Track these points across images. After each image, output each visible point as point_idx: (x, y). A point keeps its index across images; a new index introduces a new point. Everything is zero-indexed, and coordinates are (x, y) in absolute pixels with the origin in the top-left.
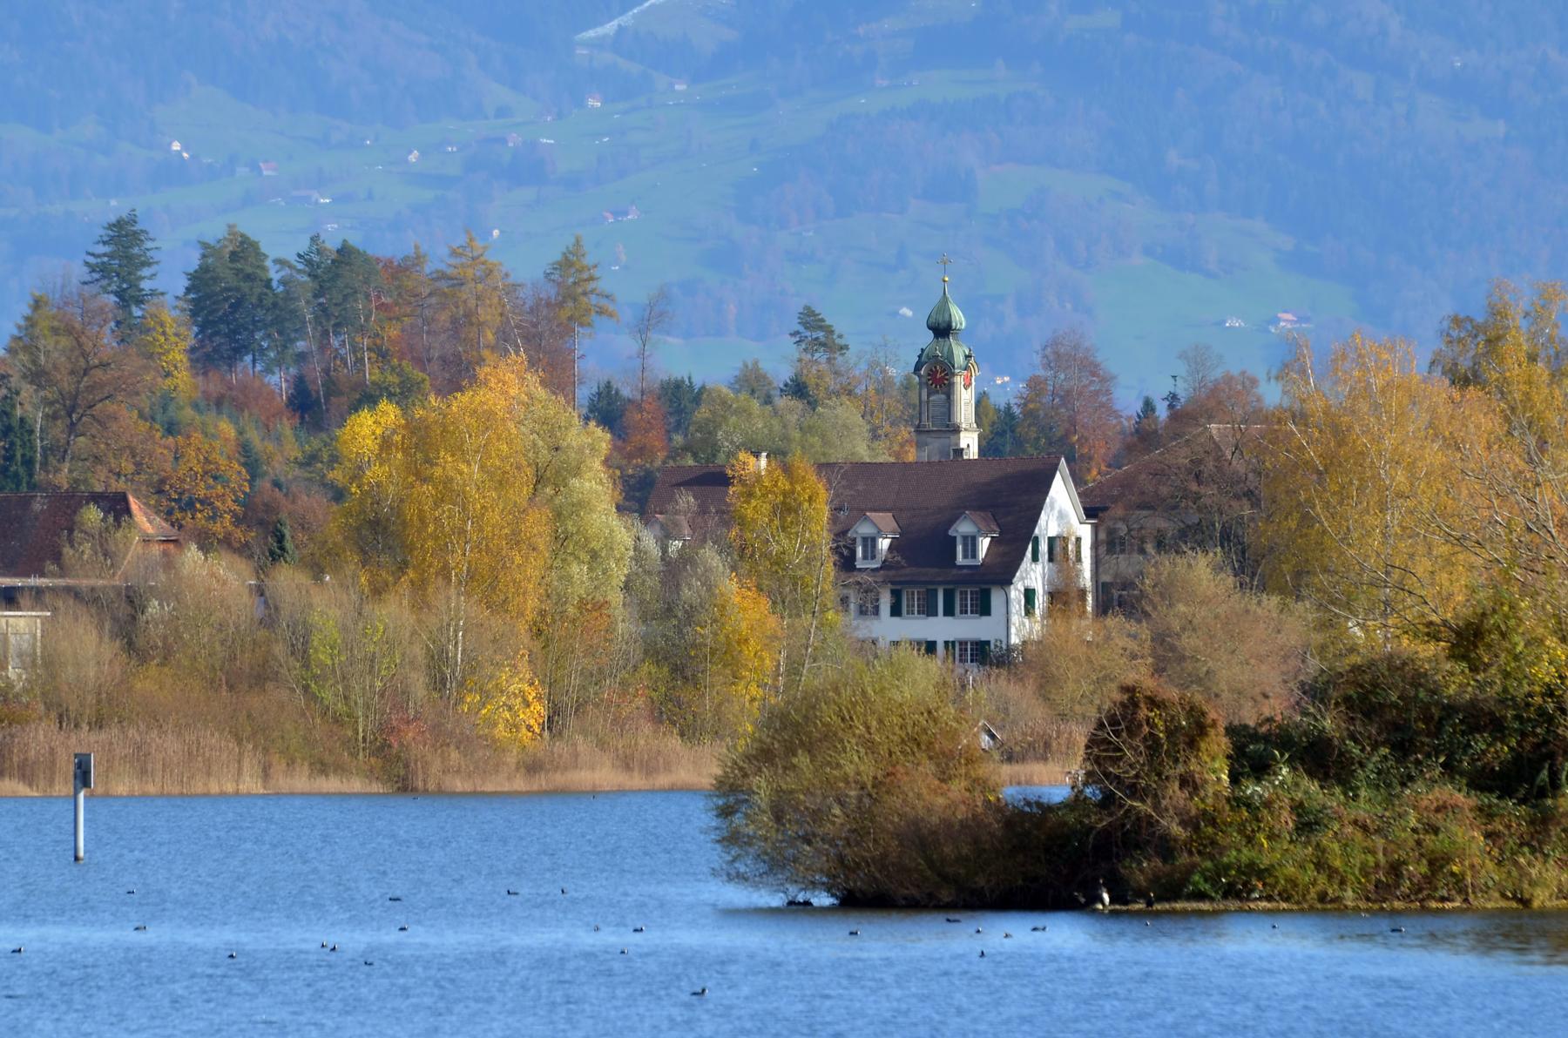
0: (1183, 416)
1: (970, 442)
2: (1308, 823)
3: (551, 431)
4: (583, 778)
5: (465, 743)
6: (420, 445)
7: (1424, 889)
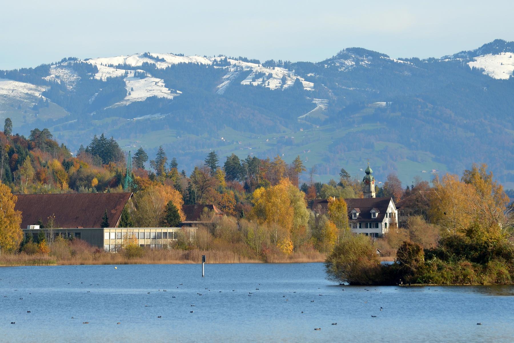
0: (414, 190)
1: (374, 195)
2: (440, 268)
4: (300, 260)
5: (278, 253)
6: (269, 195)
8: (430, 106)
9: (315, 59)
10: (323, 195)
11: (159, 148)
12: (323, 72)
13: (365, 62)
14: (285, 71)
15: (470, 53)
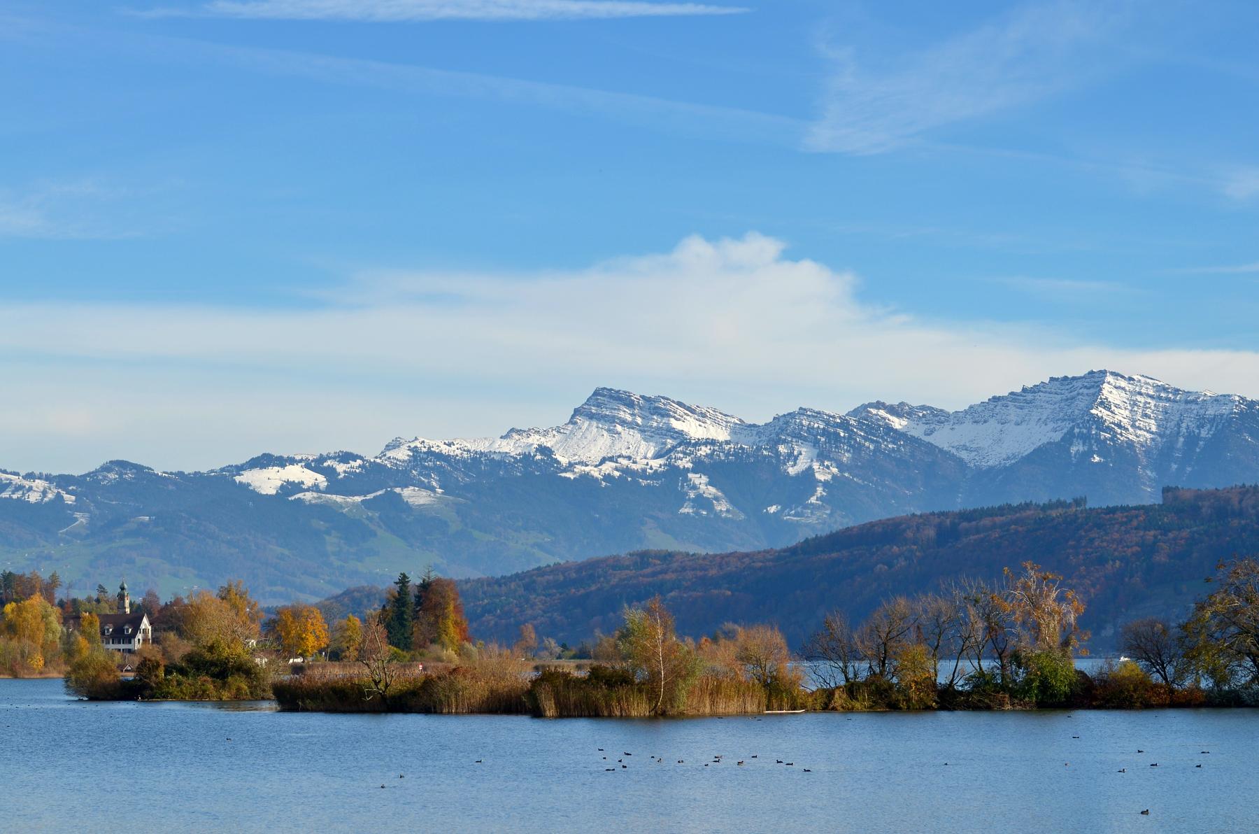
0: (172, 604)
1: (128, 610)
2: (179, 684)
3: (45, 608)
4: (51, 675)
5: (28, 669)
6: (19, 610)
7: (201, 697)
8: (194, 521)
9: (77, 472)
10: (78, 612)
11: (397, 577)
12: (86, 485)
13: (129, 476)
14: (46, 484)
15: (237, 466)
